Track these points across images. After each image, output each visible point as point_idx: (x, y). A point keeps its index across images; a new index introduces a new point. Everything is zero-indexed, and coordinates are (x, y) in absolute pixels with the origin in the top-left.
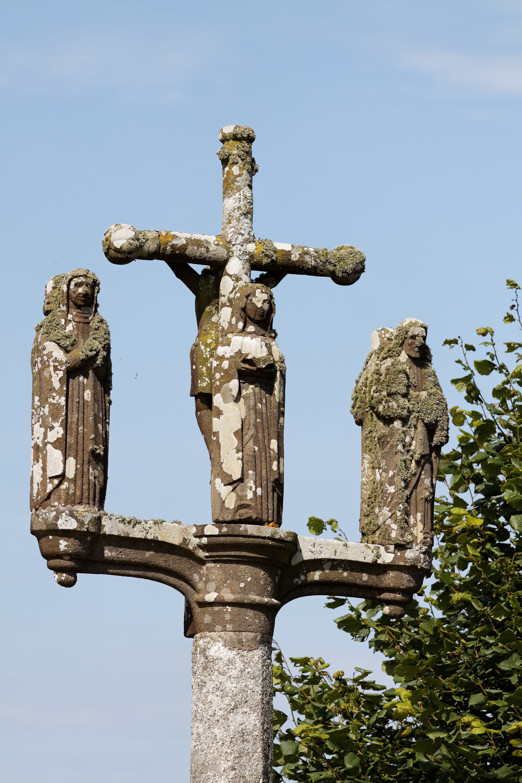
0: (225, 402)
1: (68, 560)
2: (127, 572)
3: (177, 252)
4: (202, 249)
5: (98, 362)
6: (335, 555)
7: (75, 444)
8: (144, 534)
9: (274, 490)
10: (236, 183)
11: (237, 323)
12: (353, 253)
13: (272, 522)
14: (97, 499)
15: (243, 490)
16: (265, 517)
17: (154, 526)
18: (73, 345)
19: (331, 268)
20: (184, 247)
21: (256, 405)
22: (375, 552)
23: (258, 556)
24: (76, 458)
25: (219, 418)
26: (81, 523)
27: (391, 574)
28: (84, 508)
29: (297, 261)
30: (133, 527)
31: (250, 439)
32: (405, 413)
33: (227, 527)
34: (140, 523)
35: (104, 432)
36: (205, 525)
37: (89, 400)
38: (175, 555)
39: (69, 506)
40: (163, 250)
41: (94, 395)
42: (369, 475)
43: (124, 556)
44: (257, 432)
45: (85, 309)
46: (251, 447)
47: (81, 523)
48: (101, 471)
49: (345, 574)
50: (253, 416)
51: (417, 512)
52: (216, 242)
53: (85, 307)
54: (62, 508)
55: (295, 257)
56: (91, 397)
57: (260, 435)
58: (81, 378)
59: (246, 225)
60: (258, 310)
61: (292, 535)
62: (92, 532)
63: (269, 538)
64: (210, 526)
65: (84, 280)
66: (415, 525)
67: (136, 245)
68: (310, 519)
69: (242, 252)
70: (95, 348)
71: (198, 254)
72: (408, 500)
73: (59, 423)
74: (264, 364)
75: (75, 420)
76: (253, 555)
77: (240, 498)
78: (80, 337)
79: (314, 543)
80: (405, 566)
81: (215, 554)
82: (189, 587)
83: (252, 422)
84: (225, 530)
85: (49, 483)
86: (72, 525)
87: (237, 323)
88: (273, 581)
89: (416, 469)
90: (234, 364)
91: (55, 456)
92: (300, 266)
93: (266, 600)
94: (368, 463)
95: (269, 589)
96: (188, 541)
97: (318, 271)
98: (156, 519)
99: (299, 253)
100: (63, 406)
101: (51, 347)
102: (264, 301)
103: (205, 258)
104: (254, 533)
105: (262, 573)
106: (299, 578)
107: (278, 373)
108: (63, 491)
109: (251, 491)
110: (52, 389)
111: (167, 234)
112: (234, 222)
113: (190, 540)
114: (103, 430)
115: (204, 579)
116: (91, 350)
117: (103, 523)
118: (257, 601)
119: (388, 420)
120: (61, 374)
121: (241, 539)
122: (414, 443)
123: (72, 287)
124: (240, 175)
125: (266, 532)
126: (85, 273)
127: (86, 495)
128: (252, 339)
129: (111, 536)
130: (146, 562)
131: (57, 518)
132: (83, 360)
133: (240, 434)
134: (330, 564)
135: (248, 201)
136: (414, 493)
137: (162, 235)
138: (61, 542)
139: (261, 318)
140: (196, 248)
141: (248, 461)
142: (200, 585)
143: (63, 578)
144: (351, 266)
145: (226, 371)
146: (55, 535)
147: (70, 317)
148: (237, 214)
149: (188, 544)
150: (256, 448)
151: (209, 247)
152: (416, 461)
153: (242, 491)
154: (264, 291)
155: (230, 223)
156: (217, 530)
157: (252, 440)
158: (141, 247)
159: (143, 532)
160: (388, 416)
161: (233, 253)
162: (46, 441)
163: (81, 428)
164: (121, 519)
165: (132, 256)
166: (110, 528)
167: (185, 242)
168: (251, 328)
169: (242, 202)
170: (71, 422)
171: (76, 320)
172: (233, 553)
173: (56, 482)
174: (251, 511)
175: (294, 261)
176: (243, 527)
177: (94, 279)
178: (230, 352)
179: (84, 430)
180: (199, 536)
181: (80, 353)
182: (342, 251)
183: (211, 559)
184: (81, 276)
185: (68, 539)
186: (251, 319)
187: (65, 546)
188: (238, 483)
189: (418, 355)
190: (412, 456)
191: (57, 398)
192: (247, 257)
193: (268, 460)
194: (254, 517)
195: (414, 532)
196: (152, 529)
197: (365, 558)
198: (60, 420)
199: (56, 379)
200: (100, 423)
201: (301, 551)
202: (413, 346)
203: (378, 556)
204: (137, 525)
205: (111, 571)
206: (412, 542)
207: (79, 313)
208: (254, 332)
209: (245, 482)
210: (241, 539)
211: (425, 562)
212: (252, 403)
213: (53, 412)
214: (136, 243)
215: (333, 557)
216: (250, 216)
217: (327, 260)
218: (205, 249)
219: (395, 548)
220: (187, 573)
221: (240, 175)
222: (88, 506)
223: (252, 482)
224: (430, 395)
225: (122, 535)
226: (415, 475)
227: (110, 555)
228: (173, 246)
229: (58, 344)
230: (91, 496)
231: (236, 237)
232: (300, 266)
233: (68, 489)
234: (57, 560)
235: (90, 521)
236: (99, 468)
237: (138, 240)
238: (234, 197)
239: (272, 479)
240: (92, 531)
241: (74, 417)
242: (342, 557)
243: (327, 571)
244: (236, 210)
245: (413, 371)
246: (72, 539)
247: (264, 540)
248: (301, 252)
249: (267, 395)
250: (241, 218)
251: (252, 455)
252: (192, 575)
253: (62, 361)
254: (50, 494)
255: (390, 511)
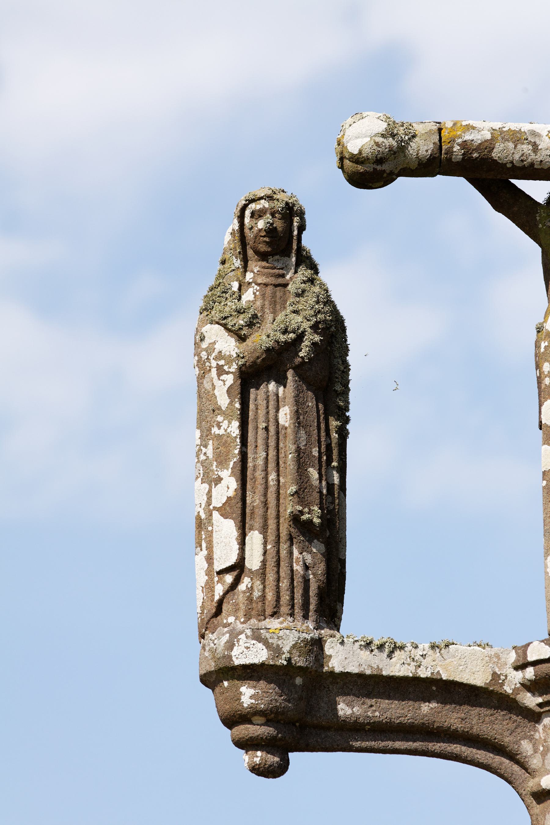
1: (261, 725)
2: (390, 744)
3: (475, 155)
4: (525, 146)
5: (301, 354)
7: (261, 506)
8: (412, 668)
14: (312, 607)
17: (431, 652)
18: (250, 325)
24: (264, 530)
28: (281, 623)
34: (402, 648)
35: (324, 483)
36: (528, 645)
37: (287, 425)
38: (481, 707)
39: (253, 621)
40: (446, 154)
41: (297, 414)
43: (377, 714)
45: (278, 260)
47: (276, 651)
48: (319, 556)
53: (277, 257)
54: (240, 626)
56: (291, 418)
58: (272, 386)
62: (300, 667)
64: (536, 643)
65: (267, 205)
67: (391, 147)
70: (294, 326)
71: (517, 157)
73: (230, 470)
75: (260, 462)
78: (267, 311)
82: (516, 768)
85: (218, 582)
86: (258, 655)
96: (502, 677)
98: (438, 641)
100: (236, 437)
101: (216, 334)
103: (532, 164)
108: (241, 595)
110: (216, 410)
111: (455, 124)
113: (506, 676)
115: (541, 749)
116: (285, 332)
117: (328, 650)
120: (230, 379)
123: (247, 220)
126: (269, 192)
127: (285, 598)
130: (423, 724)
131: (230, 646)
137: (446, 128)
138: (243, 689)
140: (511, 145)
142: (535, 761)
143: (257, 760)
147: (249, 276)
149: (502, 684)
151: (538, 143)
158: (401, 149)
159: (409, 664)
162: (211, 507)
164: (363, 643)
165: (386, 167)
166: (342, 657)
167: (488, 136)
170: (254, 466)
171: (259, 281)
173: (229, 578)
177: (287, 204)
179: (279, 481)
181: (262, 338)
184: (261, 198)
185: (255, 683)
187: (251, 697)
191: (225, 424)
196: (428, 659)
198: (231, 464)
199: (223, 388)
200: (313, 466)
204: (397, 653)
205: (357, 744)
207: (264, 267)
213: (218, 450)
220: (507, 740)
222: (291, 619)
225: (368, 672)
227: (349, 712)
228: (464, 145)
229: (225, 326)
230: (298, 600)
233: (251, 589)
234: (242, 727)
235: (294, 646)
236: (314, 550)
237: (393, 136)
240: (300, 664)
241: (257, 459)
246: (262, 683)
252: (517, 742)
253: (230, 356)
254: (220, 603)
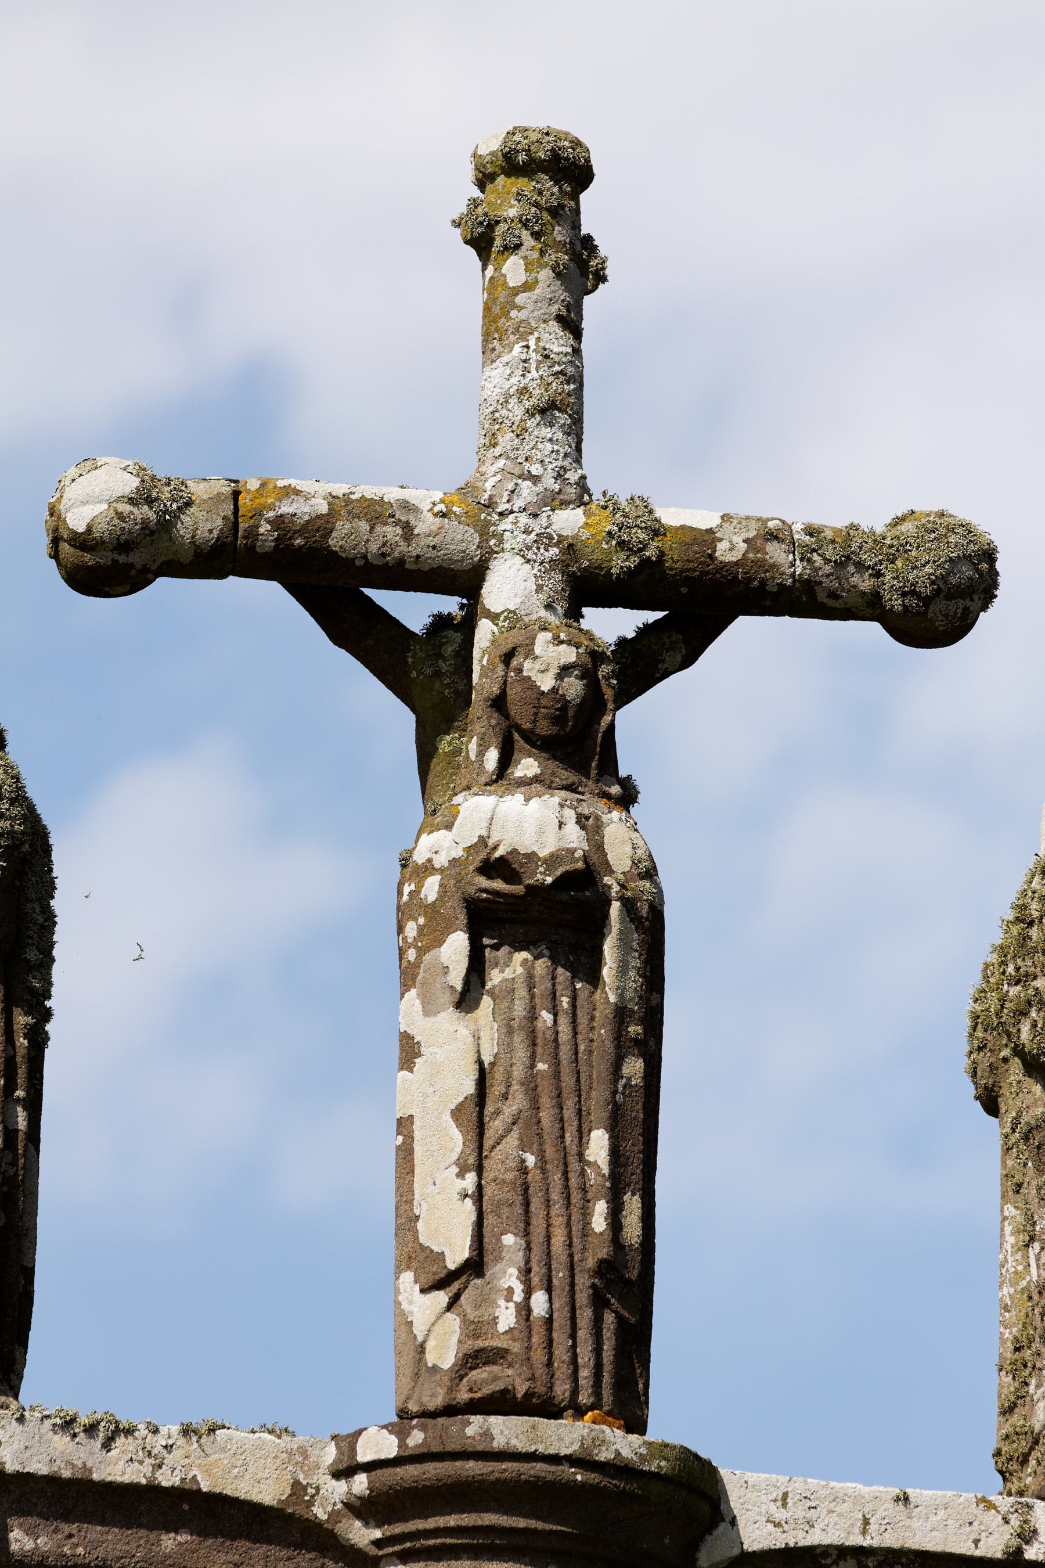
0: (427, 1013)
3: (298, 541)
4: (388, 529)
6: (864, 1532)
8: (147, 1469)
9: (599, 1302)
10: (513, 313)
11: (481, 754)
12: (939, 527)
13: (592, 1408)
15: (485, 1300)
16: (562, 1390)
17: (181, 1441)
19: (865, 583)
20: (322, 525)
22: (1015, 1521)
23: (540, 1525)
25: (411, 1071)
29: (736, 564)
30: (107, 1445)
31: (508, 1131)
33: (423, 1428)
34: (129, 1432)
36: (359, 1433)
38: (270, 1543)
40: (245, 537)
42: (1016, 1273)
43: (80, 1550)
46: (508, 1152)
50: (521, 1053)
52: (442, 507)
55: (730, 549)
57: (546, 1116)
59: (549, 447)
60: (544, 702)
61: (671, 1454)
63: (571, 1460)
64: (373, 1430)
67: (145, 522)
69: (533, 536)
71: (374, 547)
74: (549, 871)
76: (521, 1523)
77: (473, 1329)
79: (785, 1495)
81: (398, 1529)
83: (518, 1072)
84: (416, 1438)
87: (481, 754)
90: (452, 882)
92: (750, 580)
94: (1012, 1234)
97: (822, 597)
99: (744, 536)
102: (565, 670)
104: (514, 1442)
107: (615, 907)
109: (511, 1305)
111: (263, 485)
112: (506, 440)
113: (318, 1489)
121: (472, 1468)
124: (527, 287)
125: (560, 1439)
128: (527, 800)
135: (557, 368)
137: (248, 491)
139: (555, 729)
140: (364, 526)
141: (499, 1204)
144: (928, 569)
145: (432, 911)
148: (516, 411)
149: (310, 1504)
150: (531, 1160)
151: (413, 523)
153: (477, 1306)
154: (563, 636)
155: (495, 445)
156: (393, 1440)
157: (515, 1134)
158: (163, 527)
159: (141, 1462)
161: (501, 541)
164: (58, 1421)
165: (135, 558)
167: (324, 509)
168: (527, 766)
169: (534, 374)
172: (452, 1521)
174: (510, 1372)
175: (725, 565)
176: (476, 1425)
178: (449, 848)
180: (344, 1472)
183: (390, 1550)
186: (529, 737)
188: (463, 1279)
192: (554, 551)
193: (576, 1197)
194: (521, 1391)
196: (177, 1453)
197: (976, 1542)
201: (733, 1522)
204: (120, 1441)
208: (536, 779)
209: (488, 1274)
210: (472, 1468)
212: (520, 1009)
214: (145, 512)
216: (563, 418)
217: (848, 558)
218: (399, 531)
221: (527, 287)
223: (513, 1271)
225: (66, 1474)
227: (29, 1545)
228: (279, 522)
231: (511, 486)
232: (750, 580)
237: (150, 501)
238: (505, 358)
242: (891, 1540)
244: (513, 401)
247: (553, 1468)
248: (752, 534)
249: (579, 986)
250: (531, 423)
251: (513, 1183)
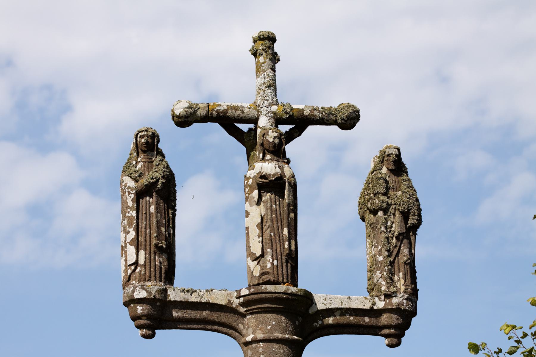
0: (250, 206)
2: (192, 326)
5: (158, 187)
8: (199, 299)
9: (287, 262)
11: (259, 155)
12: (348, 106)
15: (265, 262)
16: (280, 279)
18: (140, 176)
19: (334, 118)
20: (226, 111)
21: (271, 206)
22: (372, 301)
24: (145, 250)
26: (150, 293)
27: (385, 316)
30: (191, 294)
32: (384, 205)
33: (253, 288)
34: (195, 291)
39: (142, 283)
41: (157, 208)
44: (273, 223)
46: (268, 233)
47: (150, 293)
49: (352, 318)
50: (269, 213)
51: (399, 272)
54: (137, 284)
55: (307, 112)
57: (275, 225)
58: (148, 198)
63: (283, 293)
64: (243, 289)
66: (399, 280)
67: (191, 112)
68: (469, 344)
70: (155, 176)
71: (236, 115)
72: (392, 264)
74: (273, 177)
75: (144, 225)
77: (262, 268)
80: (392, 309)
81: (249, 308)
82: (237, 334)
83: (269, 217)
84: (252, 290)
87: (259, 155)
88: (294, 323)
89: (396, 243)
91: (131, 250)
93: (287, 336)
95: (290, 329)
98: (209, 289)
102: (275, 137)
103: (242, 118)
105: (283, 318)
106: (317, 323)
107: (287, 183)
110: (128, 207)
112: (261, 93)
114: (166, 231)
116: (152, 179)
117: (169, 293)
118: (280, 337)
119: (374, 212)
120: (132, 196)
122: (394, 225)
123: (138, 139)
124: (264, 62)
127: (153, 274)
129: (175, 302)
131: (133, 292)
132: (146, 185)
133: (261, 226)
134: (339, 312)
136: (397, 260)
138: (138, 307)
140: (234, 111)
143: (144, 333)
145: (251, 186)
146: (134, 303)
147: (139, 159)
149: (232, 304)
150: (272, 234)
152: (396, 237)
156: (248, 291)
157: (269, 229)
160: (374, 209)
163: (148, 231)
166: (173, 295)
167: (226, 108)
168: (268, 157)
171: (143, 160)
172: (260, 306)
173: (133, 267)
176: (264, 287)
180: (238, 297)
181: (144, 181)
182: (342, 106)
186: (268, 151)
189: (393, 168)
190: (393, 234)
192: (272, 114)
193: (282, 241)
194: (272, 280)
195: (398, 286)
196: (205, 295)
199: (130, 199)
201: (316, 304)
202: (389, 162)
203: (374, 304)
204: (194, 293)
205: (180, 326)
206: (397, 292)
208: (270, 159)
211: (408, 305)
212: (269, 205)
215: (340, 306)
216: (272, 88)
219: (385, 297)
220: (234, 324)
221: (264, 62)
223: (270, 256)
224: (403, 193)
225: (183, 300)
226: (396, 247)
227: (177, 315)
228: (217, 111)
229: (131, 177)
235: (156, 291)
237: (191, 108)
239: (285, 254)
241: (142, 224)
242: (347, 306)
243: (338, 317)
245: (391, 179)
246: (145, 305)
250: (266, 89)
252: (238, 325)
254: (130, 276)
255: (380, 273)
